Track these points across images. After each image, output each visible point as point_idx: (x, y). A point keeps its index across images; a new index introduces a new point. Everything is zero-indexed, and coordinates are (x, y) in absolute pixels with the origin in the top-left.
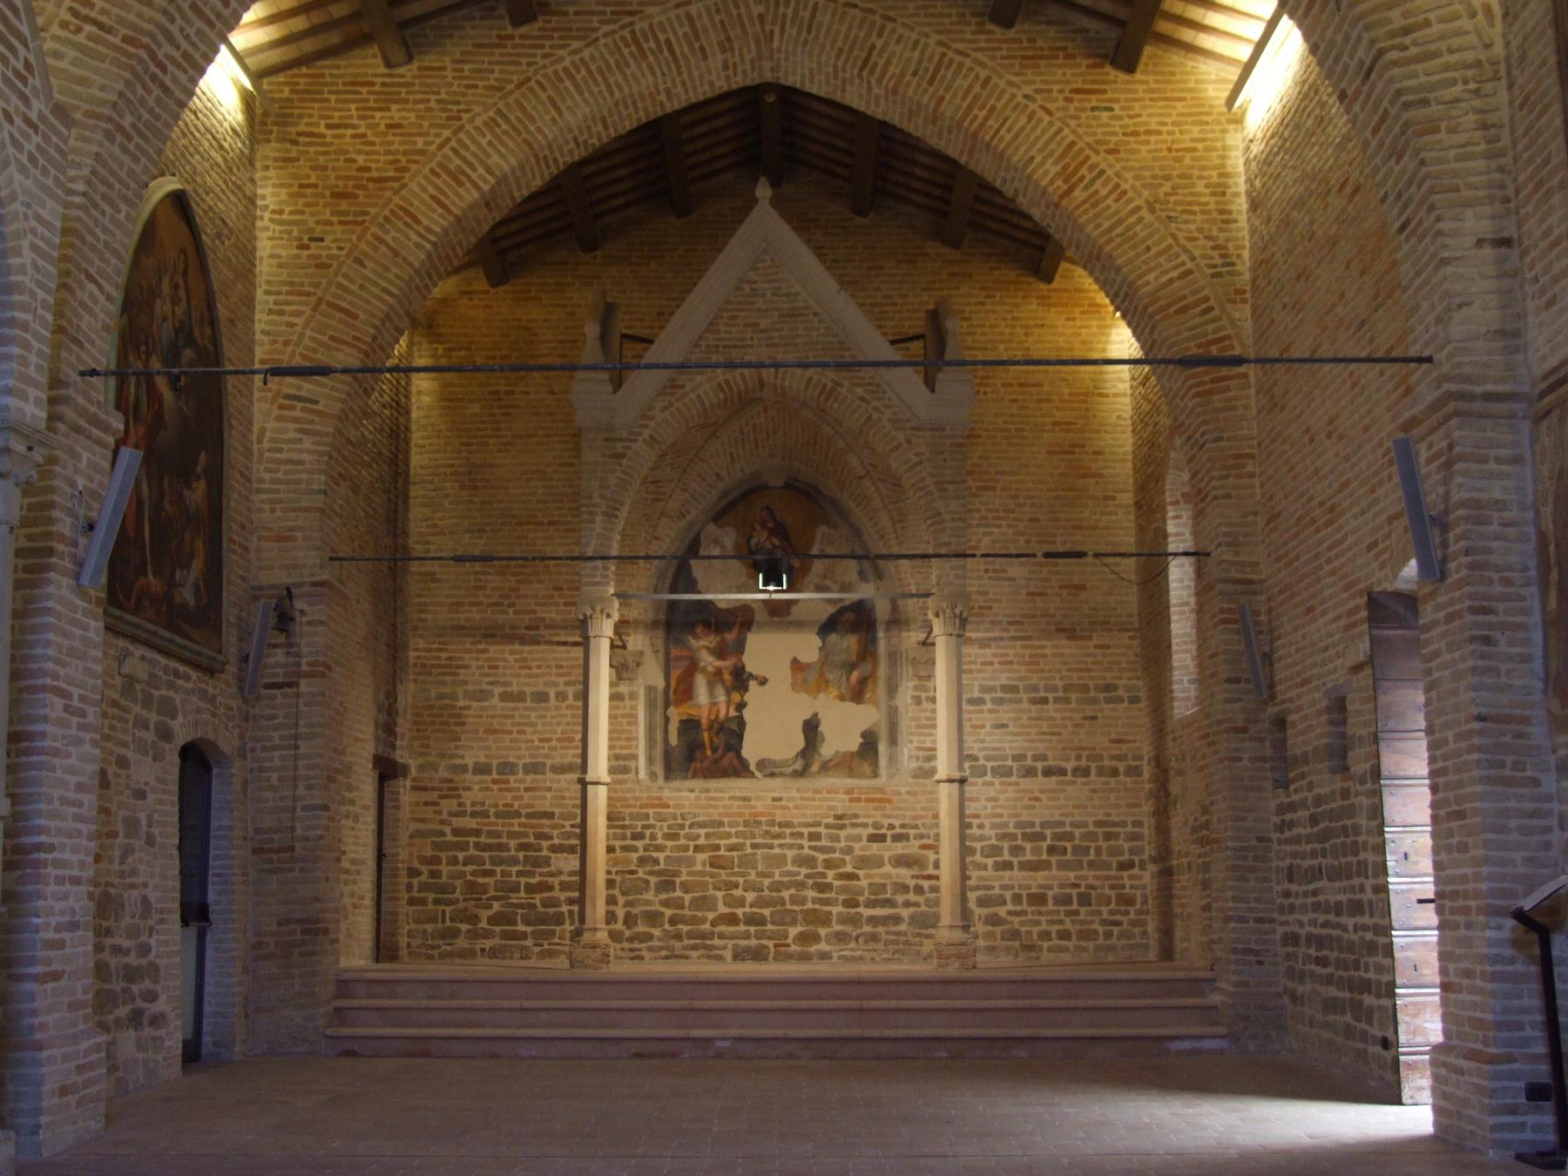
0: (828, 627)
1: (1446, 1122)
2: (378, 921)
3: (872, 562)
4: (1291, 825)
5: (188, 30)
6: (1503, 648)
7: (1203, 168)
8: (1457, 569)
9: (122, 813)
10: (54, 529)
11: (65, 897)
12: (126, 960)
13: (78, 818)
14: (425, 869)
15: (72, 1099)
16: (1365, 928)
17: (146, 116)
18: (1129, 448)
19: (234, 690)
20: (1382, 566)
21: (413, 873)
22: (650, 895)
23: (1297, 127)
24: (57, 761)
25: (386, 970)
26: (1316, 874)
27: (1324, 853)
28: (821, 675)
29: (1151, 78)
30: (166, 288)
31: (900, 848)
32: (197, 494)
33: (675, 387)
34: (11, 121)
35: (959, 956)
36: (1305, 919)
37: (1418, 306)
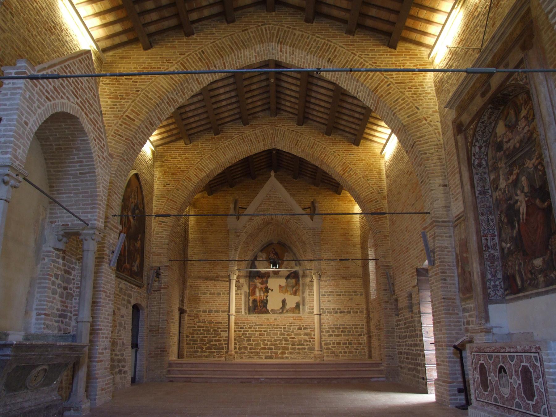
0: (288, 277)
3: (298, 262)
4: (400, 325)
6: (448, 281)
8: (437, 263)
11: (104, 342)
12: (118, 357)
13: (108, 322)
16: (418, 350)
20: (420, 262)
21: (187, 336)
22: (245, 343)
23: (397, 159)
24: (103, 308)
26: (406, 337)
30: (133, 196)
31: (305, 331)
32: (138, 245)
36: (403, 348)
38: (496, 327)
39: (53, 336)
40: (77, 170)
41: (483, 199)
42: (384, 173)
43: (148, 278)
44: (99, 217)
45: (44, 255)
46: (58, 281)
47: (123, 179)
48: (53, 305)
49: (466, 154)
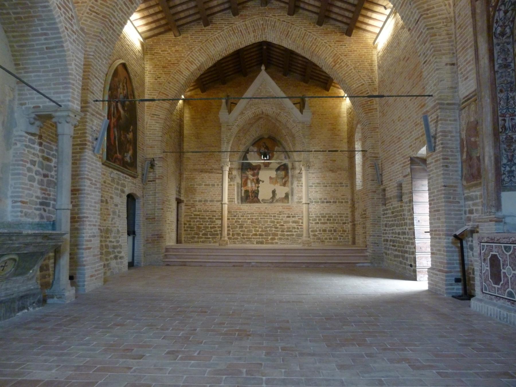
0: (278, 169)
1: (432, 287)
2: (177, 235)
3: (287, 153)
4: (386, 214)
5: (119, 15)
6: (451, 168)
7: (367, 59)
8: (438, 148)
9: (112, 210)
10: (87, 139)
11: (92, 229)
12: (113, 244)
13: (95, 210)
14: (188, 223)
15: (94, 278)
16: (406, 238)
17: (109, 37)
18: (346, 129)
19: (140, 182)
20: (413, 151)
21: (185, 224)
22: (237, 229)
23: (392, 47)
24: (88, 196)
25: (179, 246)
26: (393, 225)
27: (395, 221)
28: (276, 180)
29: (355, 38)
30: (121, 86)
31: (294, 219)
33: (243, 113)
34: (68, 30)
35: (307, 244)
36: (390, 236)
37: (428, 82)
38: (509, 216)
39: (29, 224)
40: (43, 44)
41: (504, 74)
42: (376, 64)
43: (143, 169)
44: (74, 98)
45: (15, 140)
46: (36, 168)
47: (104, 63)
48: (31, 192)
49: (486, 22)
